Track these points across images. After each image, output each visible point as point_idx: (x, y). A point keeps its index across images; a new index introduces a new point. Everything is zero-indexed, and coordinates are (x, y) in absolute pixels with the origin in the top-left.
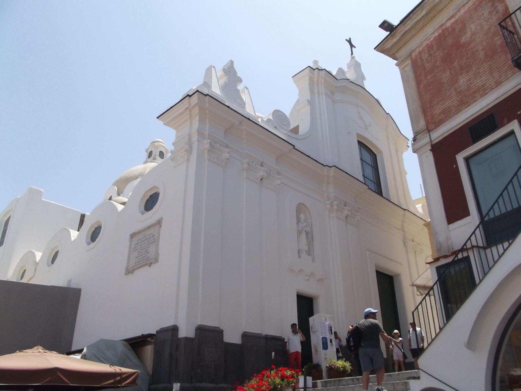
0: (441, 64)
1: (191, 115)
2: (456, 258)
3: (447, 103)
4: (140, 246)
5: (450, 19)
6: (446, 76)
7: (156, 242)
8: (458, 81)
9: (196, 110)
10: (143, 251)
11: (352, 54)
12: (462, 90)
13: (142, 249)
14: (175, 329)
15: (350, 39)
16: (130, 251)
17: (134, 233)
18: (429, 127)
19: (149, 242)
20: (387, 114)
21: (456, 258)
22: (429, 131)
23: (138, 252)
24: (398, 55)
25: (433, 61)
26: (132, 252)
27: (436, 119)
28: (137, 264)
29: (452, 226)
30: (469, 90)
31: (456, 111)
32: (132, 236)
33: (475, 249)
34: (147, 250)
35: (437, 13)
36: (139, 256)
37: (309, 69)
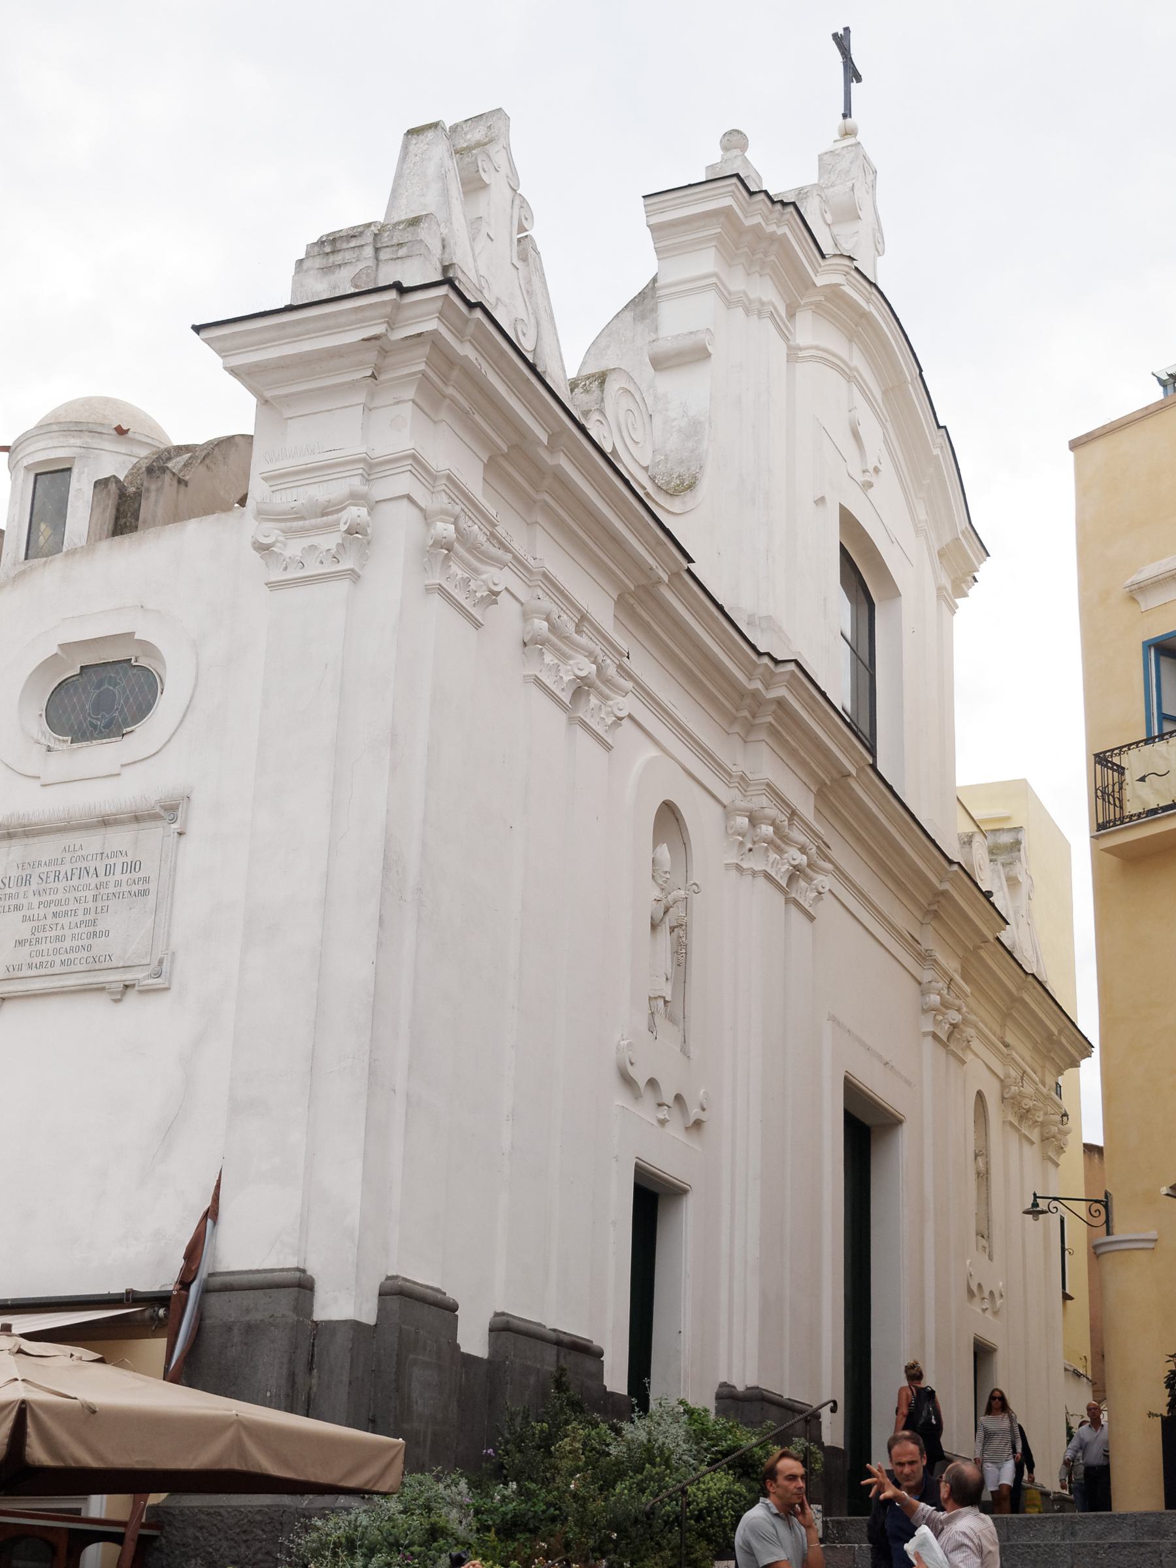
7: (152, 897)
10: (65, 921)
15: (847, 29)
20: (939, 427)
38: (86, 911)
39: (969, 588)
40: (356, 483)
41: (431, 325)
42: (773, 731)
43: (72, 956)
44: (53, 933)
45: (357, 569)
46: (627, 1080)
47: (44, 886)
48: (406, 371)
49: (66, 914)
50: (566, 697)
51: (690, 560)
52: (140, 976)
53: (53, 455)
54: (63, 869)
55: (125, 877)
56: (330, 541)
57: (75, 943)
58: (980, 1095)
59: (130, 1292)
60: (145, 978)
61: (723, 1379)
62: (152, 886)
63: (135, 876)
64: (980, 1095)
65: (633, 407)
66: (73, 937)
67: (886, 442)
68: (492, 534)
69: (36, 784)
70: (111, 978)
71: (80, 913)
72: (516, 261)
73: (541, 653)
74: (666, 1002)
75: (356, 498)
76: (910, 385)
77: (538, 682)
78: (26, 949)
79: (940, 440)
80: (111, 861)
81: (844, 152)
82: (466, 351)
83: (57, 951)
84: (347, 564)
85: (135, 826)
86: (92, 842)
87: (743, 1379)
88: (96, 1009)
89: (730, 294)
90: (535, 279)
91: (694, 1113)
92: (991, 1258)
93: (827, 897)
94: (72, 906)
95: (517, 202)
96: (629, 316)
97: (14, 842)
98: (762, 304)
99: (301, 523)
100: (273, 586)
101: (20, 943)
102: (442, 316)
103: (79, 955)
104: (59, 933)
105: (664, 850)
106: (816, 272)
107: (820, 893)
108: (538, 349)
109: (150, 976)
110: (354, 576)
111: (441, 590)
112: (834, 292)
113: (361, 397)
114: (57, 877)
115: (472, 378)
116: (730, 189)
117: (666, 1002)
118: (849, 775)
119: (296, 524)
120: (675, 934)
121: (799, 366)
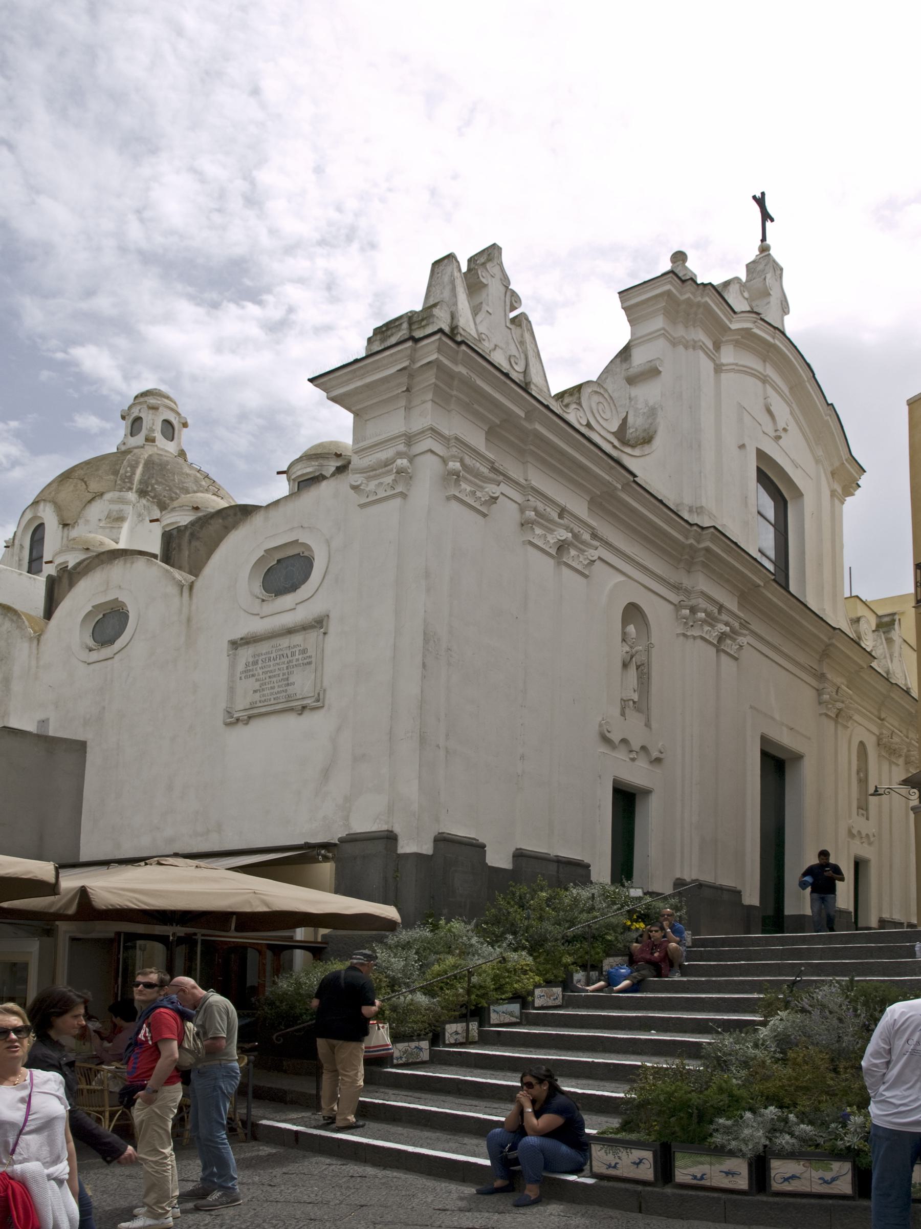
7: (313, 665)
10: (274, 679)
11: (764, 239)
14: (390, 838)
15: (763, 194)
20: (828, 405)
26: (241, 678)
34: (287, 679)
36: (263, 690)
38: (284, 674)
39: (855, 491)
40: (402, 448)
41: (434, 357)
42: (705, 565)
43: (278, 695)
44: (269, 686)
45: (404, 492)
46: (606, 740)
47: (264, 664)
48: (426, 384)
49: (274, 676)
50: (553, 551)
51: (635, 476)
52: (309, 702)
53: (305, 471)
54: (272, 656)
55: (300, 657)
56: (389, 479)
57: (279, 689)
58: (862, 744)
59: (306, 844)
60: (312, 703)
61: (678, 876)
62: (313, 660)
63: (305, 656)
64: (862, 744)
65: (602, 400)
66: (279, 686)
67: (791, 413)
68: (492, 467)
69: (258, 617)
70: (296, 704)
71: (281, 675)
72: (508, 325)
73: (533, 529)
74: (634, 702)
75: (400, 455)
76: (807, 384)
77: (531, 543)
78: (258, 694)
79: (829, 412)
80: (294, 650)
81: (761, 260)
82: (461, 369)
83: (272, 694)
84: (399, 489)
85: (304, 632)
86: (285, 642)
87: (689, 874)
88: (291, 720)
89: (674, 339)
90: (527, 336)
91: (655, 754)
92: (867, 819)
93: (746, 647)
94: (277, 673)
95: (509, 293)
96: (618, 360)
97: (250, 646)
98: (695, 342)
99: (374, 472)
100: (362, 506)
101: (255, 691)
102: (439, 350)
103: (281, 695)
104: (272, 685)
105: (631, 629)
106: (731, 321)
107: (741, 646)
108: (527, 371)
109: (314, 702)
110: (403, 495)
111: (456, 498)
112: (747, 332)
113: (403, 403)
114: (270, 660)
115: (467, 384)
116: (670, 279)
117: (634, 702)
118: (759, 586)
119: (372, 474)
120: (640, 669)
121: (723, 376)
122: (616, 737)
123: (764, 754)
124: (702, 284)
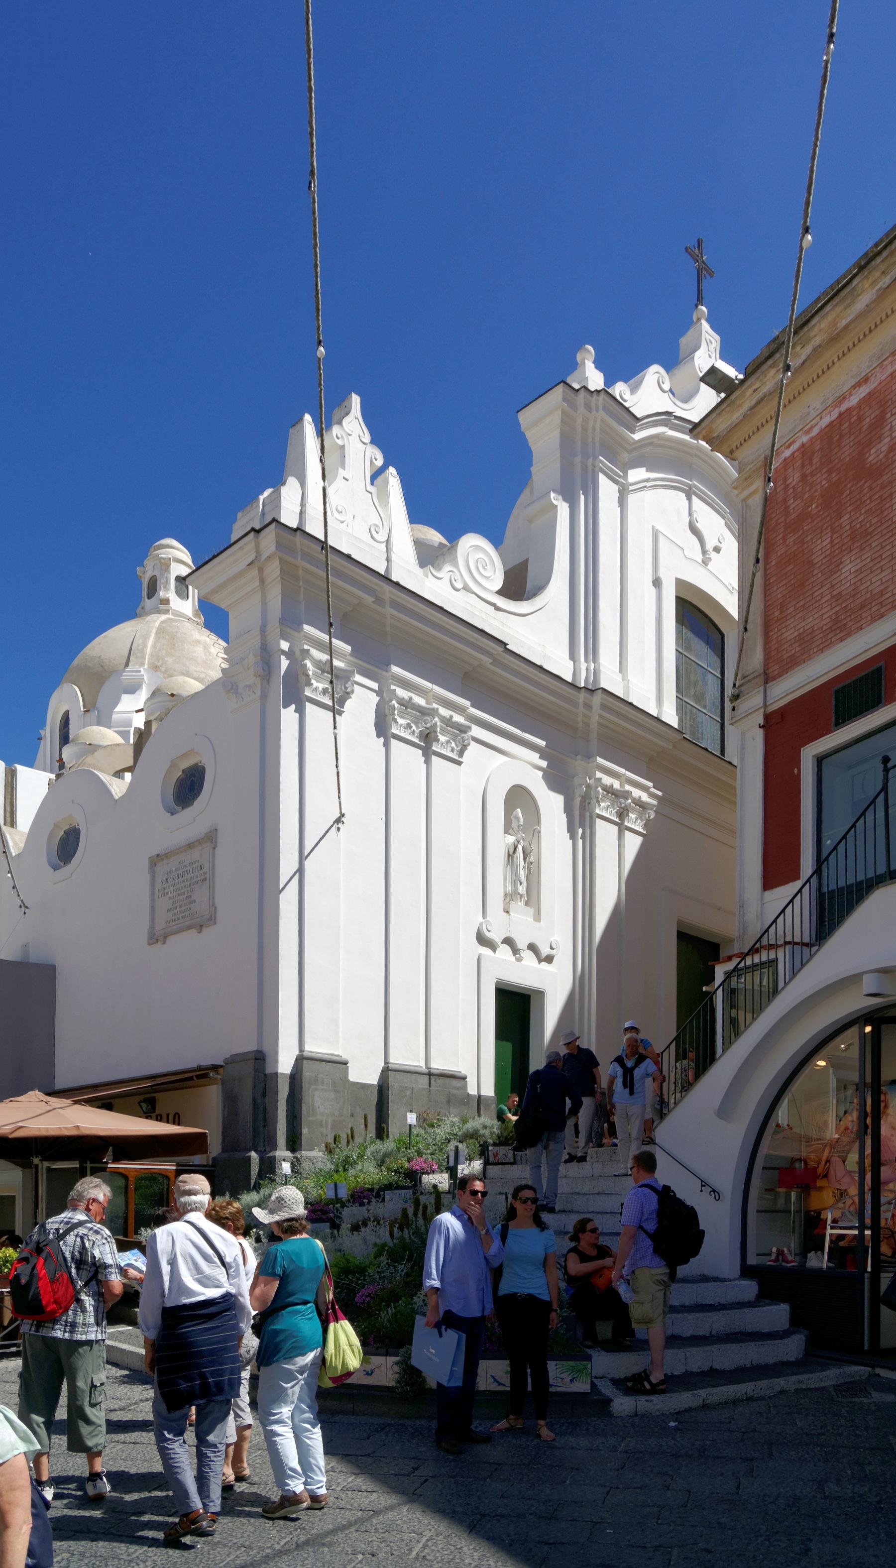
0: (819, 511)
1: (262, 580)
2: (742, 965)
3: (811, 619)
4: (173, 886)
5: (858, 385)
6: (821, 545)
8: (841, 566)
9: (273, 570)
10: (181, 897)
12: (844, 593)
13: (178, 892)
16: (152, 894)
17: (158, 855)
18: (768, 669)
19: (192, 878)
21: (742, 965)
22: (766, 682)
23: (170, 898)
24: (740, 454)
25: (807, 495)
27: (785, 652)
28: (172, 924)
29: (768, 894)
30: (854, 595)
31: (822, 643)
32: (155, 861)
33: (787, 947)
34: (190, 897)
35: (836, 359)
36: (174, 909)
37: (564, 391)
38: (188, 891)
78: (171, 913)
83: (180, 912)
101: (169, 910)
103: (186, 913)
122: (496, 936)
123: (682, 936)
124: (596, 391)
